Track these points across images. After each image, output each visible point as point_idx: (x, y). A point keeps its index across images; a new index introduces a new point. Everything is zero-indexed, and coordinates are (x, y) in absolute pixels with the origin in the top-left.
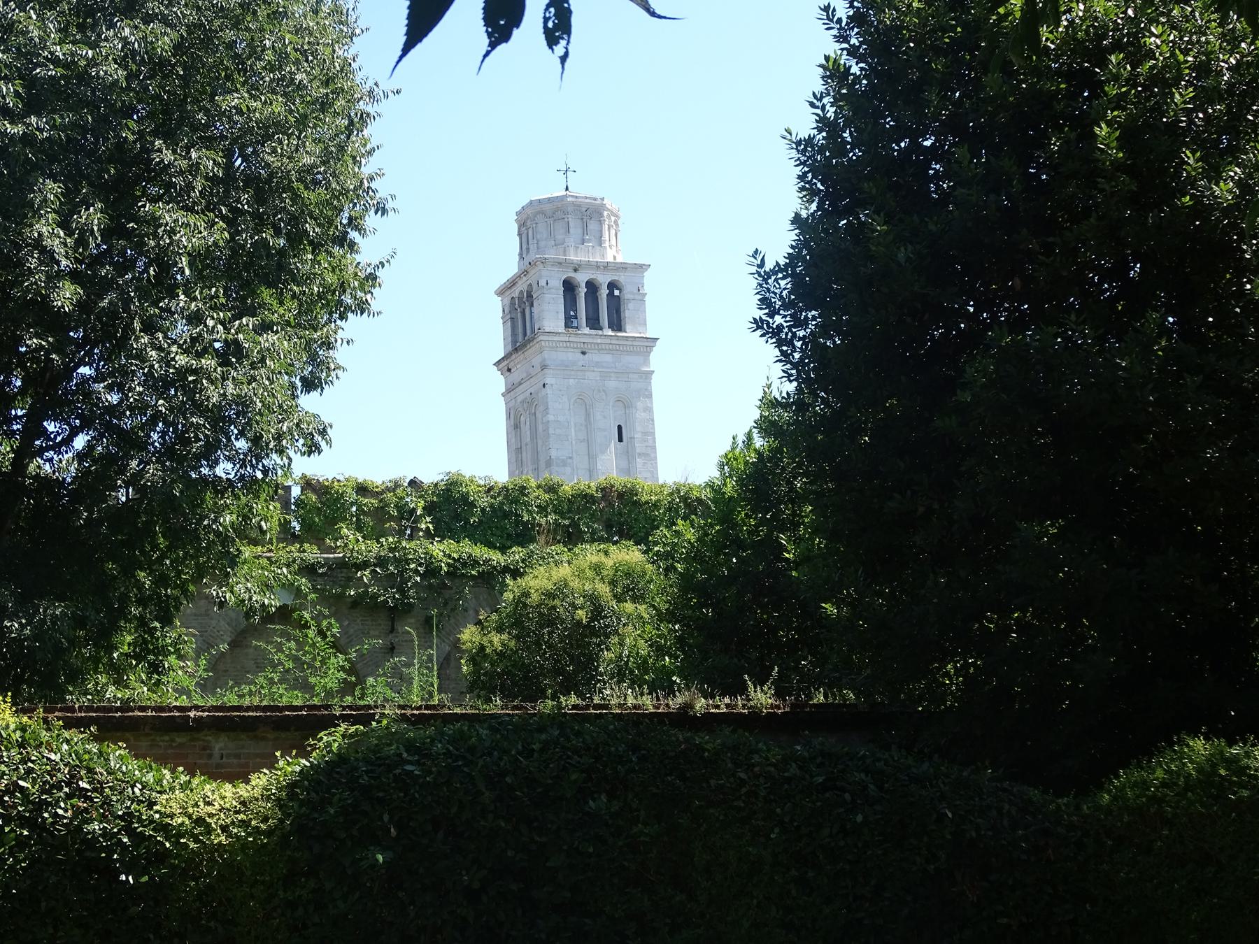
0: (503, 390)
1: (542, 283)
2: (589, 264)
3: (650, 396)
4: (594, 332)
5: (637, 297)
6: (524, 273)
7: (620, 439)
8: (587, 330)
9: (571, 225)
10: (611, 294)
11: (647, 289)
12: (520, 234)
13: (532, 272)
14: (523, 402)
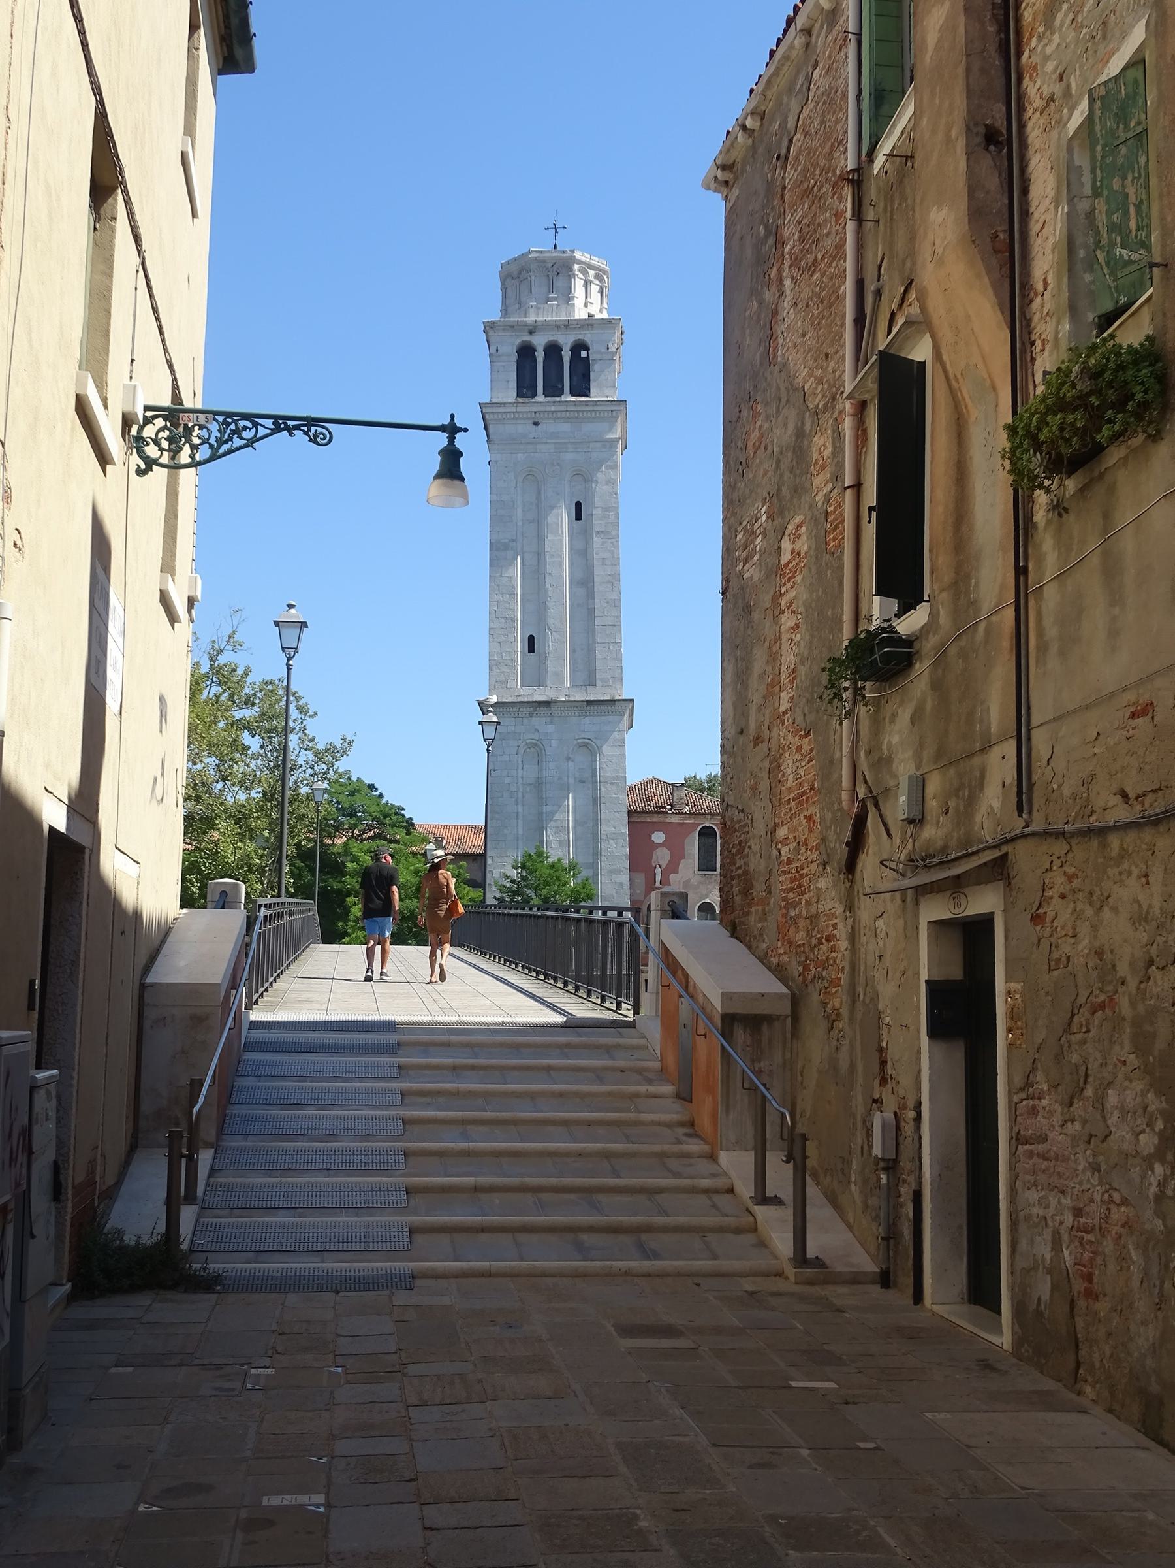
5: (605, 357)
7: (578, 516)
8: (541, 398)
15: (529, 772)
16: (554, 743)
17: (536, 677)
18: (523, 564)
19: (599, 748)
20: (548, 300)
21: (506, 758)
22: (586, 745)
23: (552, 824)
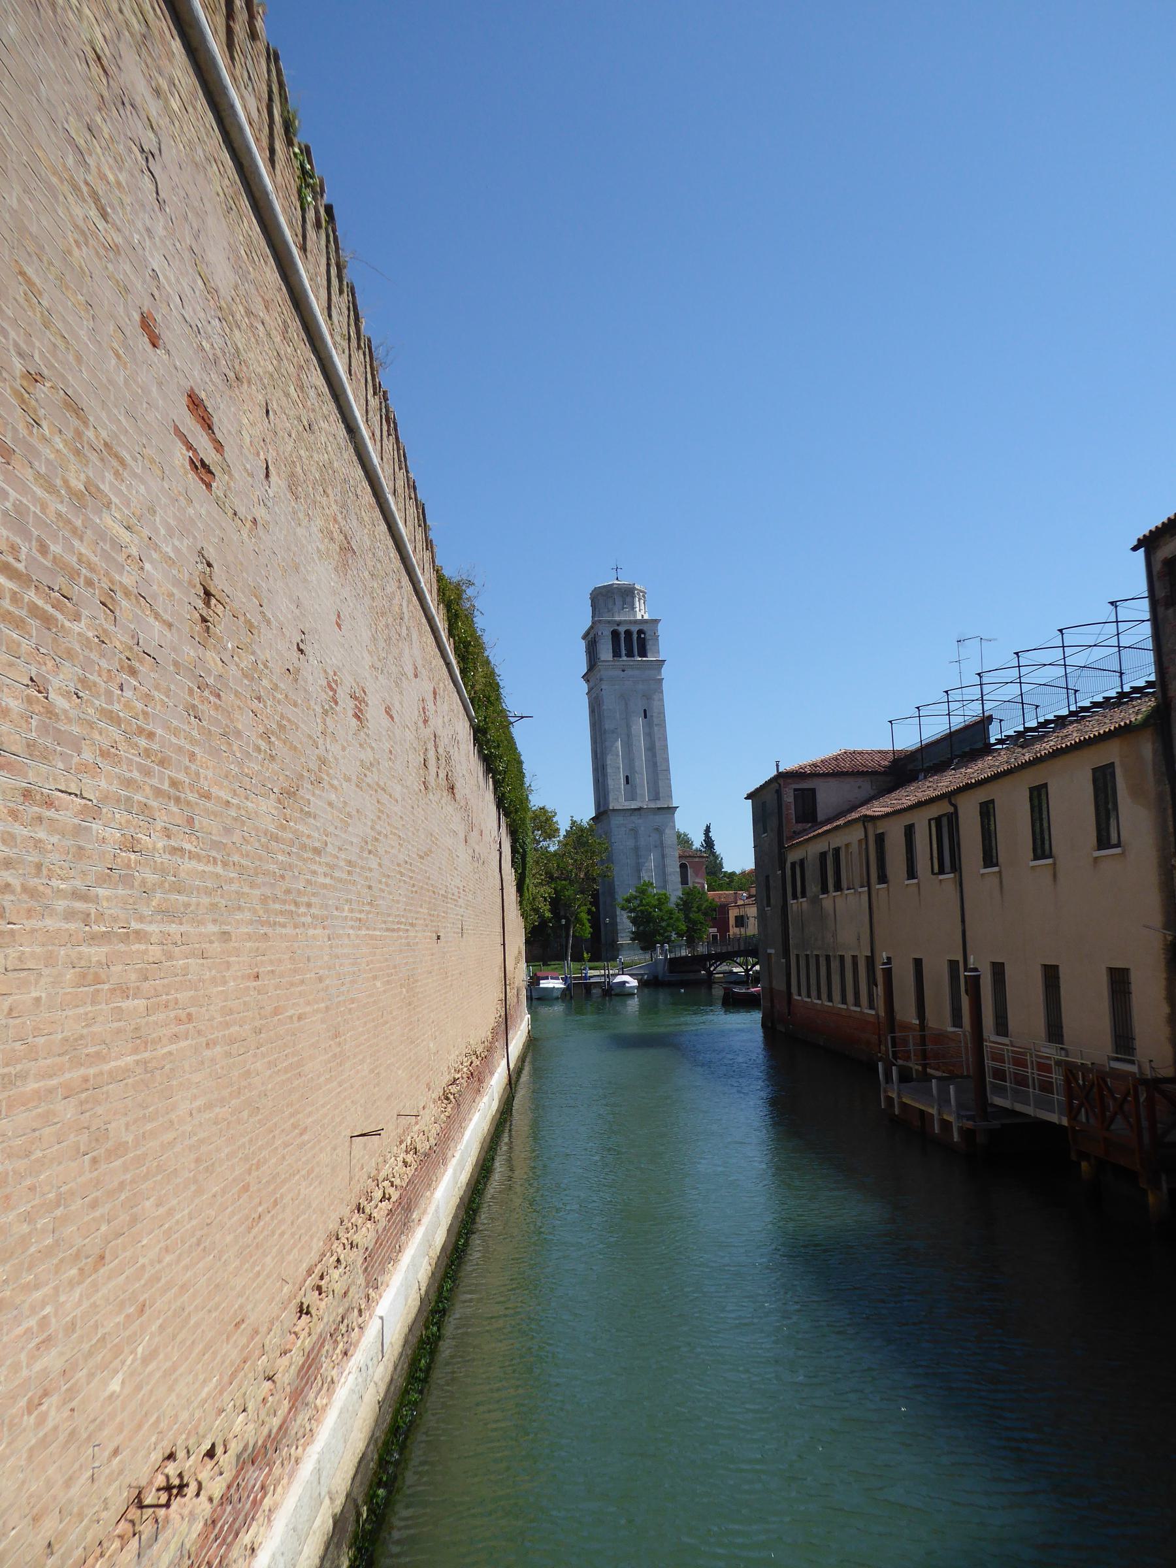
6: (592, 627)
8: (625, 658)
10: (639, 637)
11: (659, 633)
15: (630, 843)
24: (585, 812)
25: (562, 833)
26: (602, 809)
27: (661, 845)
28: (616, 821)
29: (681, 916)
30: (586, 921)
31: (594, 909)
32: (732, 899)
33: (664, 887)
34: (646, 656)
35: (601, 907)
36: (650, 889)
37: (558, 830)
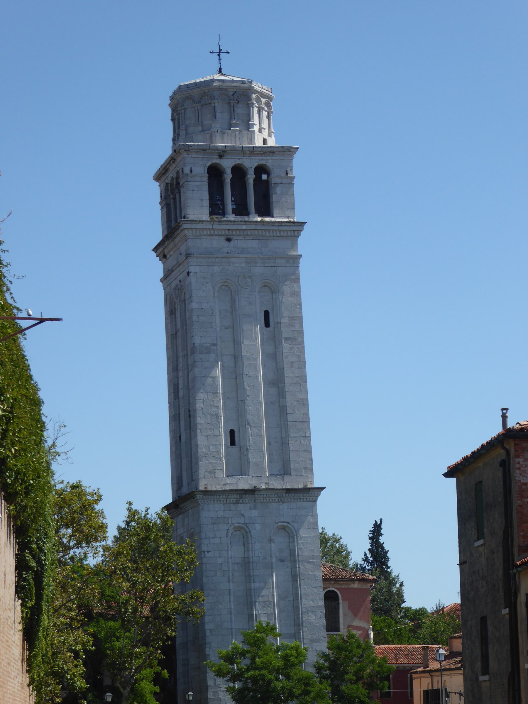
0: (161, 275)
1: (187, 171)
2: (234, 150)
3: (297, 280)
4: (239, 218)
5: (285, 181)
6: (172, 160)
7: (267, 324)
8: (232, 217)
9: (218, 110)
10: (258, 179)
12: (173, 119)
13: (179, 159)
14: (175, 289)
15: (236, 553)
16: (258, 526)
17: (240, 469)
18: (222, 366)
19: (297, 531)
20: (230, 126)
21: (217, 541)
22: (284, 528)
23: (260, 599)
24: (155, 495)
25: (112, 532)
26: (185, 490)
27: (291, 558)
28: (210, 512)
29: (326, 688)
30: (149, 697)
31: (165, 673)
32: (418, 658)
33: (296, 635)
34: (269, 213)
35: (180, 669)
36: (270, 639)
37: (103, 527)
